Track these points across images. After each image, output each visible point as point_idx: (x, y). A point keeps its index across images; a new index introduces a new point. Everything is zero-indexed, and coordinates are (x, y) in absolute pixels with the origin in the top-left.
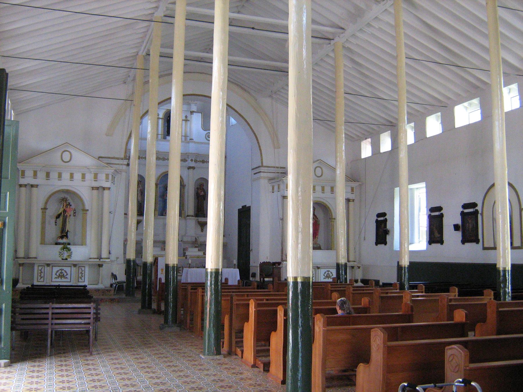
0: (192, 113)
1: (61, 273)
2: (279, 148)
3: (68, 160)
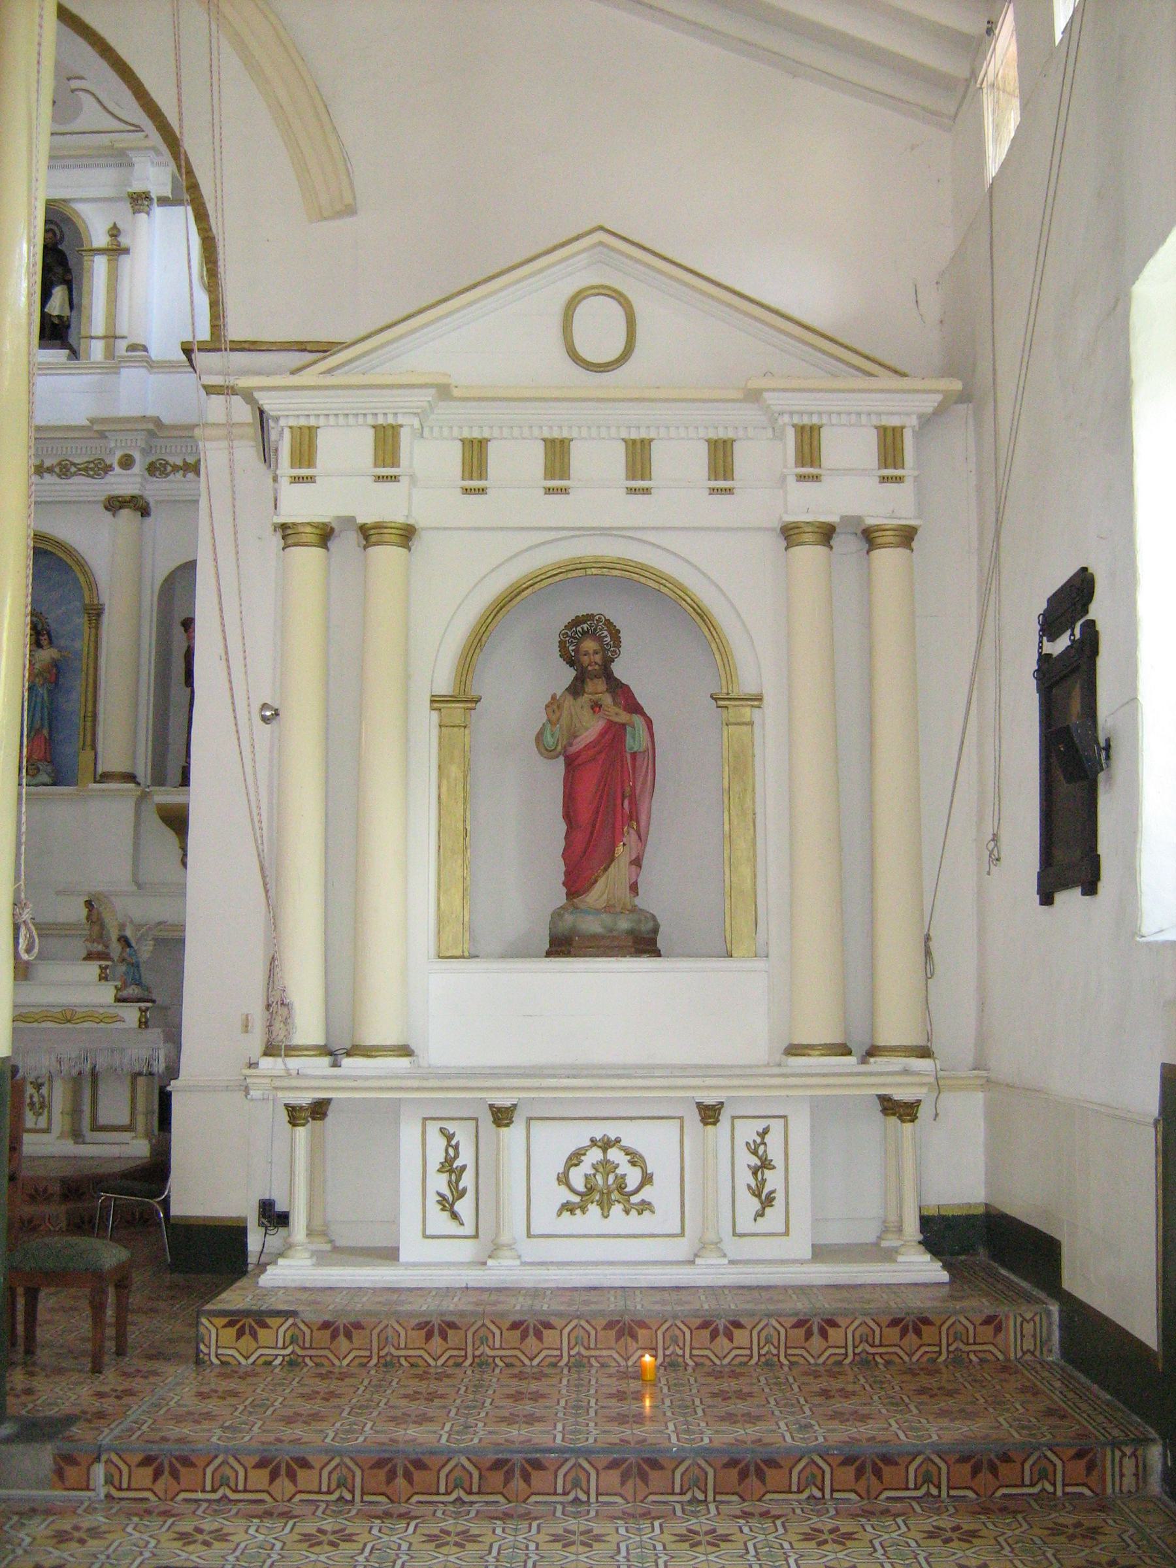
0: (140, 201)
1: (606, 1166)
2: (350, 211)
3: (614, 350)
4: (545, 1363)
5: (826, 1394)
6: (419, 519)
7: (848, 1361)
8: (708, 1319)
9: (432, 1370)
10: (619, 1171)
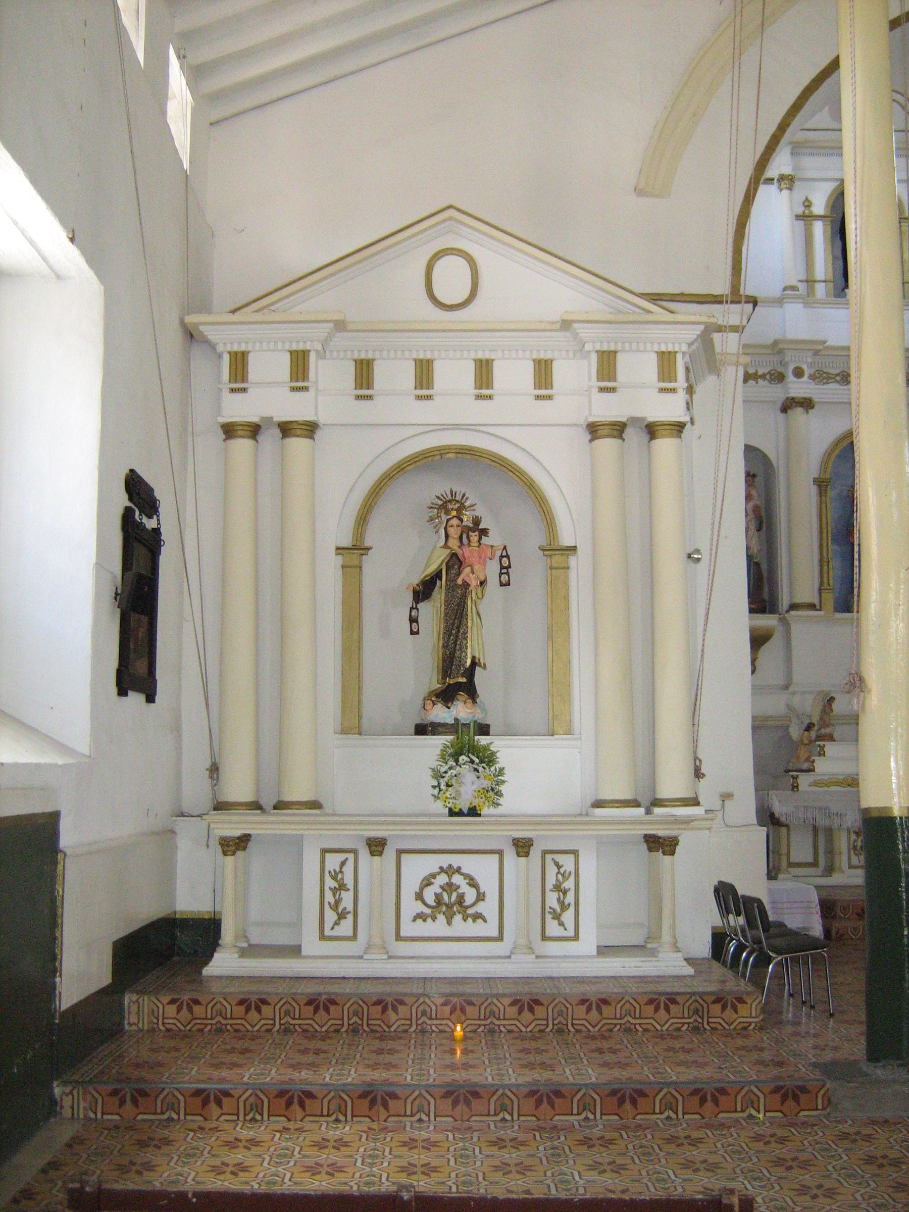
1: (450, 887)
3: (465, 294)
4: (672, 1028)
5: (600, 1051)
6: (322, 419)
7: (548, 1030)
8: (312, 997)
9: (318, 1034)
10: (460, 891)
